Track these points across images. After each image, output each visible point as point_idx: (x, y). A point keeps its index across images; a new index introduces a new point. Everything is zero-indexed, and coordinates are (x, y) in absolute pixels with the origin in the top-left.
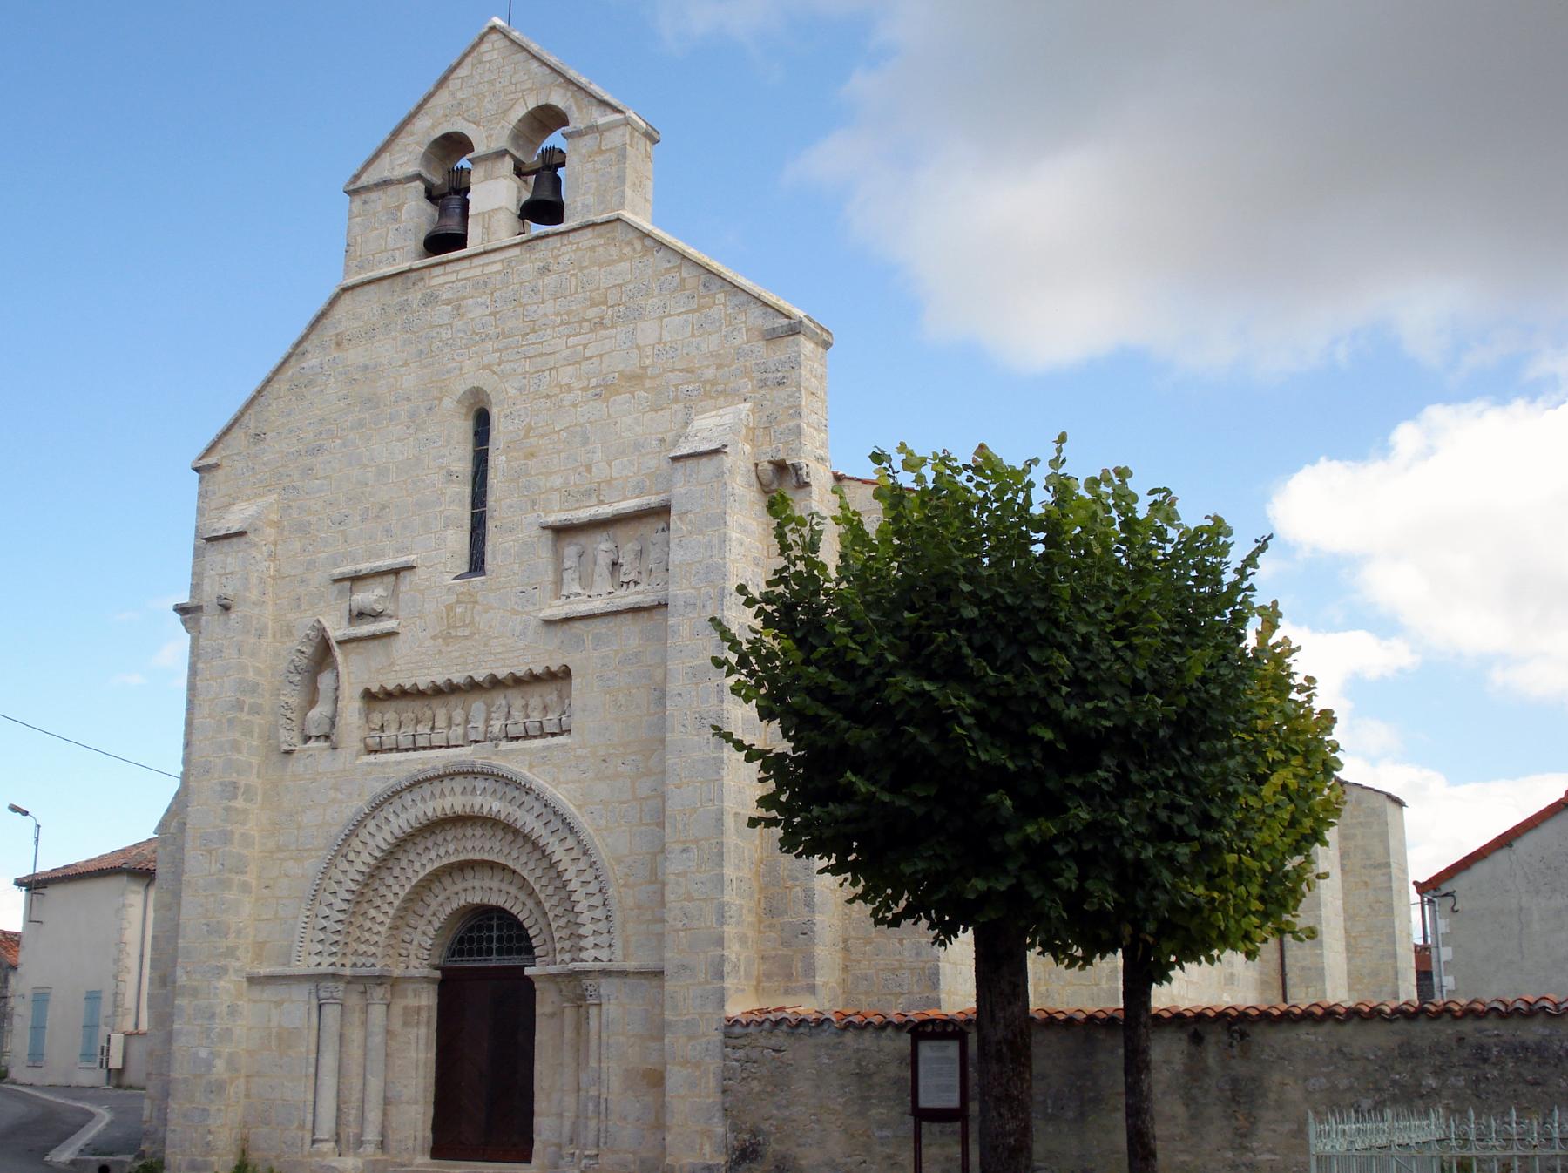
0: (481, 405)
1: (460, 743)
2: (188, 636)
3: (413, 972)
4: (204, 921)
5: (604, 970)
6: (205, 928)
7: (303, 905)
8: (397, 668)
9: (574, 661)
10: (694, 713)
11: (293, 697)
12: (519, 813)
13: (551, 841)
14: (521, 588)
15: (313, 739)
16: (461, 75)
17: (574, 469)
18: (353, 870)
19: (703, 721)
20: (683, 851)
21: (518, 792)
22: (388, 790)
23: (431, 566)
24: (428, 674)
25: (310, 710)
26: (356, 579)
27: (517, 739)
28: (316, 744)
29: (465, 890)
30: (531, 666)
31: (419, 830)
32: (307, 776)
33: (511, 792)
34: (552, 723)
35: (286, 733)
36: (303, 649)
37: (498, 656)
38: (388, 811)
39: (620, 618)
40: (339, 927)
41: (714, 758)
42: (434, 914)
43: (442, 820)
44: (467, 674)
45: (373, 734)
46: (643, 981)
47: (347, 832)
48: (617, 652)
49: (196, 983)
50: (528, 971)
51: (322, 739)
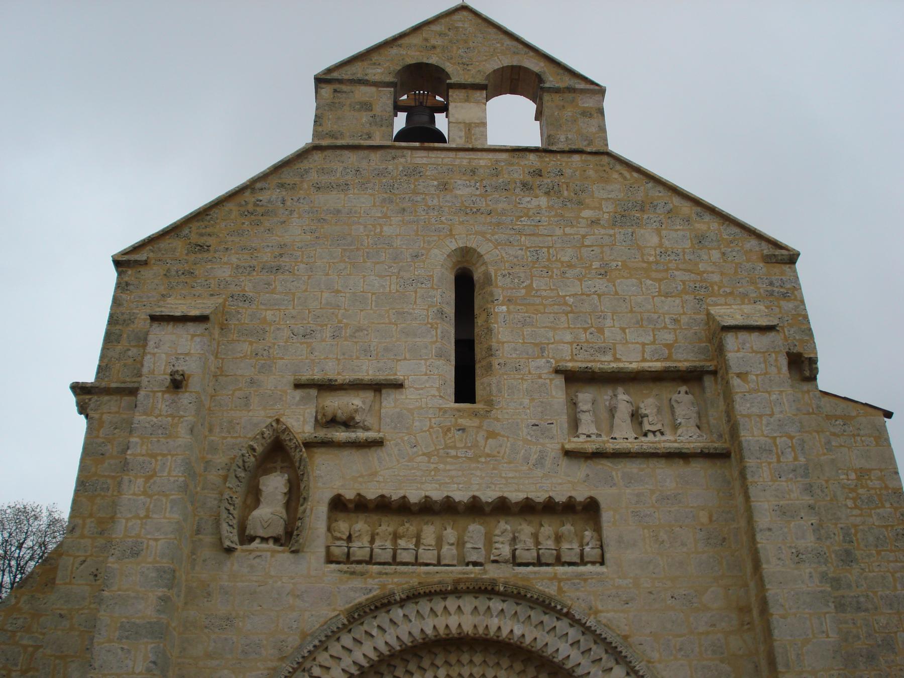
0: (465, 265)
2: (81, 423)
8: (381, 479)
9: (603, 495)
10: (790, 547)
11: (237, 492)
12: (549, 639)
15: (258, 540)
16: (432, 29)
17: (585, 330)
19: (800, 556)
21: (547, 616)
26: (327, 387)
27: (527, 565)
28: (264, 546)
30: (551, 494)
31: (393, 655)
32: (254, 578)
33: (536, 615)
35: (228, 528)
36: (255, 446)
38: (424, 606)
41: (821, 592)
51: (271, 542)
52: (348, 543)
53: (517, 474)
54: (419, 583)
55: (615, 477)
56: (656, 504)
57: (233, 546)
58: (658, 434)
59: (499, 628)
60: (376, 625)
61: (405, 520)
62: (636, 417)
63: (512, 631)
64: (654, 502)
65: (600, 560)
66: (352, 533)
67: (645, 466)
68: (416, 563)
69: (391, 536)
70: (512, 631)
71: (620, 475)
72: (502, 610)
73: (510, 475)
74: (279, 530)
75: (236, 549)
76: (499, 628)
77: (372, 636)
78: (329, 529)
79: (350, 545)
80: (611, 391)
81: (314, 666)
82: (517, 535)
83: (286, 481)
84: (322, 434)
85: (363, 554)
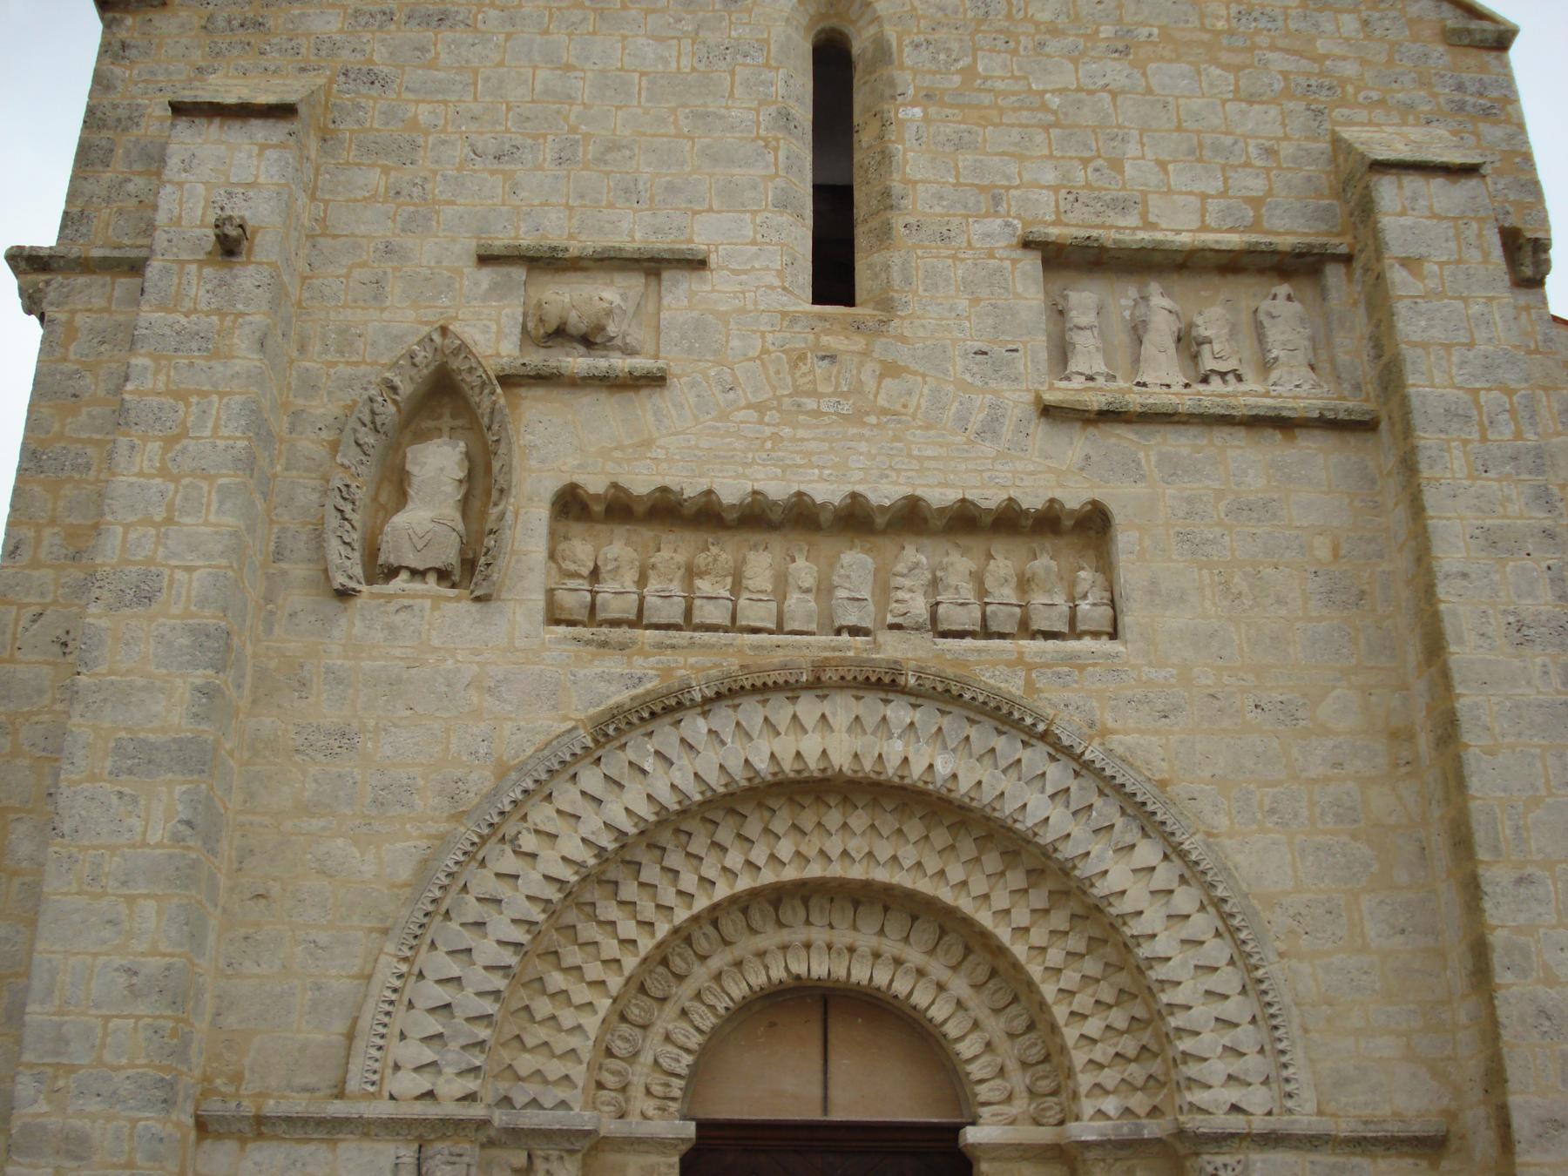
0: (834, 22)
1: (813, 627)
3: (635, 1126)
4: (118, 961)
5: (1273, 1132)
6: (122, 980)
7: (390, 947)
9: (1119, 497)
10: (1505, 612)
13: (1095, 849)
14: (978, 345)
15: (404, 575)
17: (1085, 162)
18: (536, 876)
19: (1525, 631)
20: (1520, 881)
22: (667, 696)
23: (746, 272)
24: (744, 476)
25: (397, 511)
29: (784, 948)
34: (1054, 612)
36: (397, 381)
39: (1221, 436)
40: (489, 1007)
42: (698, 996)
43: (793, 782)
44: (848, 489)
45: (572, 584)
46: (1356, 1160)
47: (530, 784)
48: (1220, 495)
49: (86, 1124)
50: (972, 1135)
51: (432, 578)
54: (742, 667)
55: (1143, 462)
58: (1230, 377)
61: (710, 540)
62: (1188, 343)
63: (931, 766)
65: (1110, 630)
66: (599, 563)
67: (1205, 442)
68: (734, 626)
70: (931, 766)
71: (1153, 459)
72: (912, 724)
73: (929, 453)
74: (449, 555)
76: (906, 760)
77: (644, 772)
78: (552, 556)
79: (597, 587)
81: (525, 832)
82: (939, 574)
84: (537, 359)
85: (623, 606)
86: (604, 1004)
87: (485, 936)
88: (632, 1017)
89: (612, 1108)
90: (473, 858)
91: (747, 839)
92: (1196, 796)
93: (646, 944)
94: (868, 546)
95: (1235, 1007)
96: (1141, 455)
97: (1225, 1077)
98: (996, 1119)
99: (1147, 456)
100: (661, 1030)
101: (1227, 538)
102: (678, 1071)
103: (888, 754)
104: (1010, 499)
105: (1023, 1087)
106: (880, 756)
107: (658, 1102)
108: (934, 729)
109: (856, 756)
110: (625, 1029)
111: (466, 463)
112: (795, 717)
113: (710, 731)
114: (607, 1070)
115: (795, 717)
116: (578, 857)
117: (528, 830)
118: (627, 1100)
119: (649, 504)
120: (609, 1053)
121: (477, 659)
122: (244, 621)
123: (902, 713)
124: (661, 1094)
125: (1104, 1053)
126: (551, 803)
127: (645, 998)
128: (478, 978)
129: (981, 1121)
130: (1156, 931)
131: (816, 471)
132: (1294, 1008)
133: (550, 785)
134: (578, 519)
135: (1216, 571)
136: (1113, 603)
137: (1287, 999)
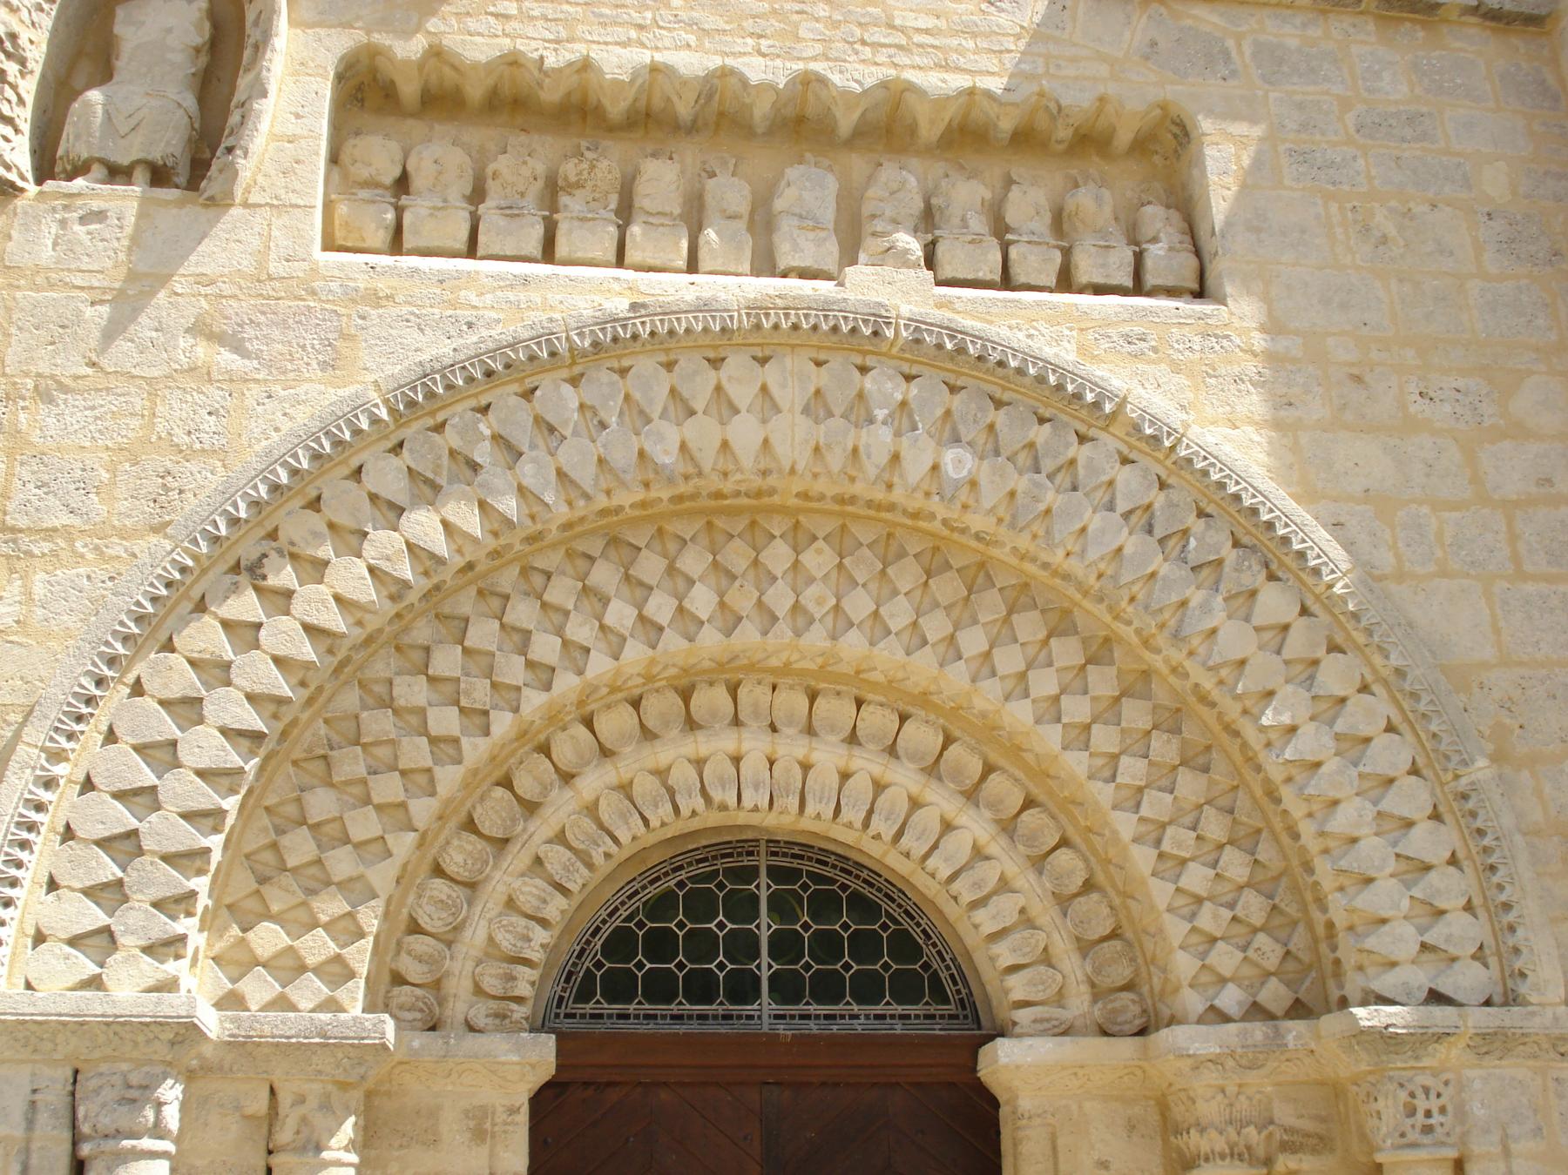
37: (918, 38)
52: (397, 197)
53: (942, 24)
54: (634, 307)
55: (1234, 54)
56: (1357, 136)
57: (20, 183)
59: (896, 458)
60: (487, 432)
61: (584, 144)
63: (935, 468)
64: (1352, 130)
65: (1195, 286)
66: (409, 168)
67: (1319, 33)
69: (540, 184)
70: (935, 468)
71: (1247, 49)
72: (904, 404)
73: (921, 24)
74: (168, 143)
75: (22, 190)
76: (896, 458)
77: (475, 467)
78: (334, 159)
79: (404, 200)
80: (208, 1055)
81: (273, 555)
83: (204, 14)
86: (402, 845)
87: (201, 721)
88: (451, 869)
89: (418, 1015)
90: (186, 596)
91: (641, 584)
92: (1342, 520)
93: (475, 749)
94: (827, 162)
95: (1427, 842)
96: (1230, 43)
97: (1418, 947)
98: (1040, 1027)
99: (1239, 46)
100: (501, 888)
101: (1361, 161)
102: (528, 954)
103: (868, 446)
104: (1041, 94)
105: (1080, 977)
106: (855, 451)
107: (493, 1005)
108: (939, 412)
109: (817, 449)
110: (439, 887)
111: (207, 26)
112: (719, 389)
113: (582, 406)
114: (409, 953)
115: (719, 389)
116: (362, 597)
117: (280, 552)
118: (441, 1002)
119: (490, 82)
120: (415, 928)
121: (208, 290)
122: (409, 1010)
123: (889, 385)
124: (499, 992)
125: (1216, 916)
126: (318, 511)
127: (473, 838)
128: (184, 789)
129: (1018, 1030)
130: (1297, 722)
131: (749, 41)
132: (1518, 838)
133: (318, 483)
134: (379, 111)
135: (1349, 206)
136: (1198, 253)
137: (1507, 821)
